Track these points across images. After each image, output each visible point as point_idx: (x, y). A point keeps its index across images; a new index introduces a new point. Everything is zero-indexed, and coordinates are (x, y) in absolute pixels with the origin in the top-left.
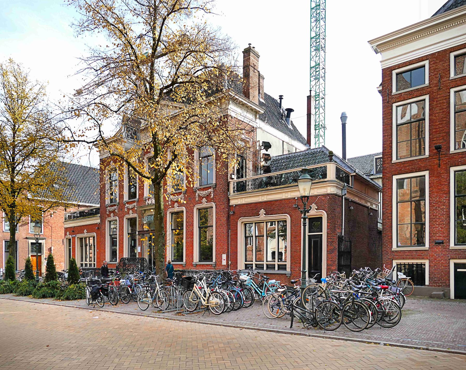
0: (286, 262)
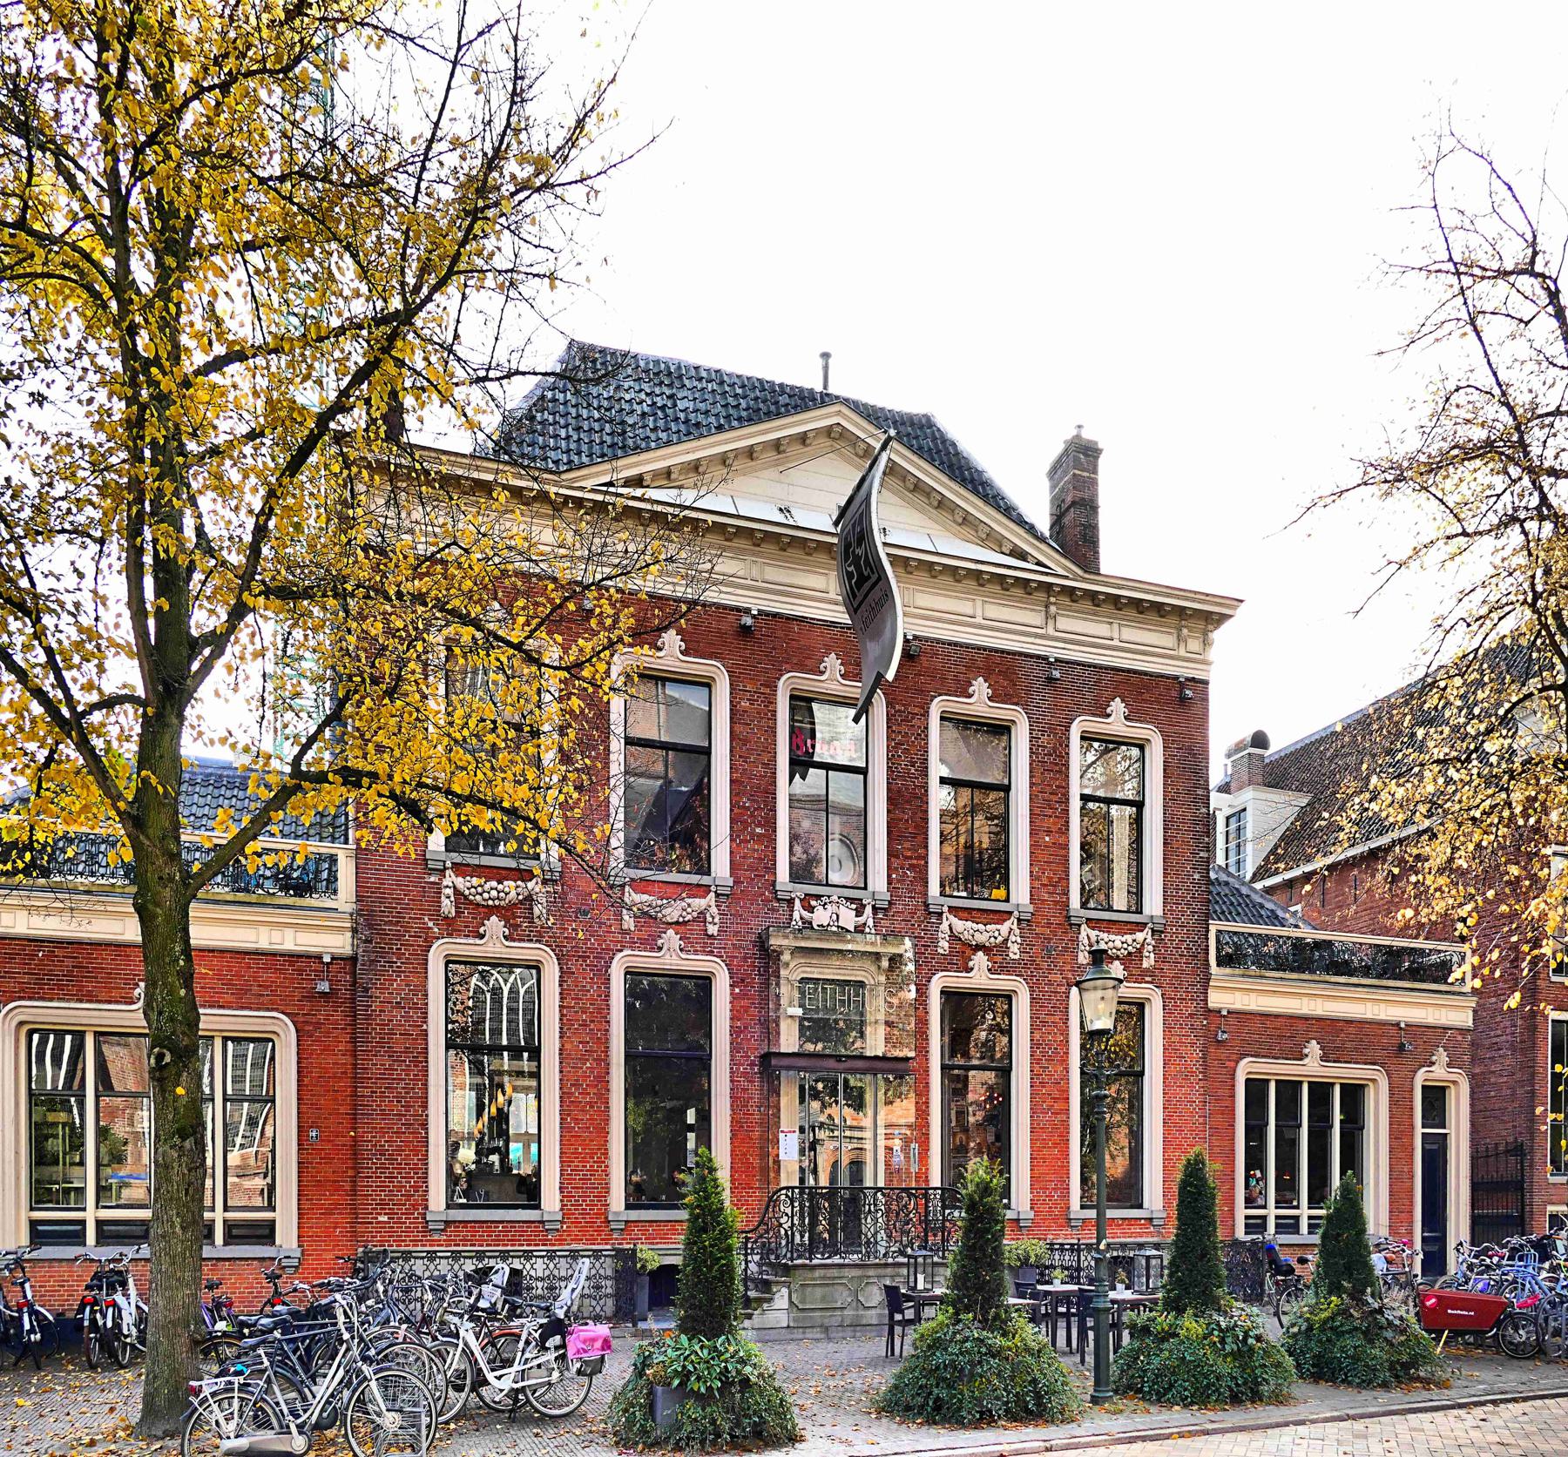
0: (274, 1210)
